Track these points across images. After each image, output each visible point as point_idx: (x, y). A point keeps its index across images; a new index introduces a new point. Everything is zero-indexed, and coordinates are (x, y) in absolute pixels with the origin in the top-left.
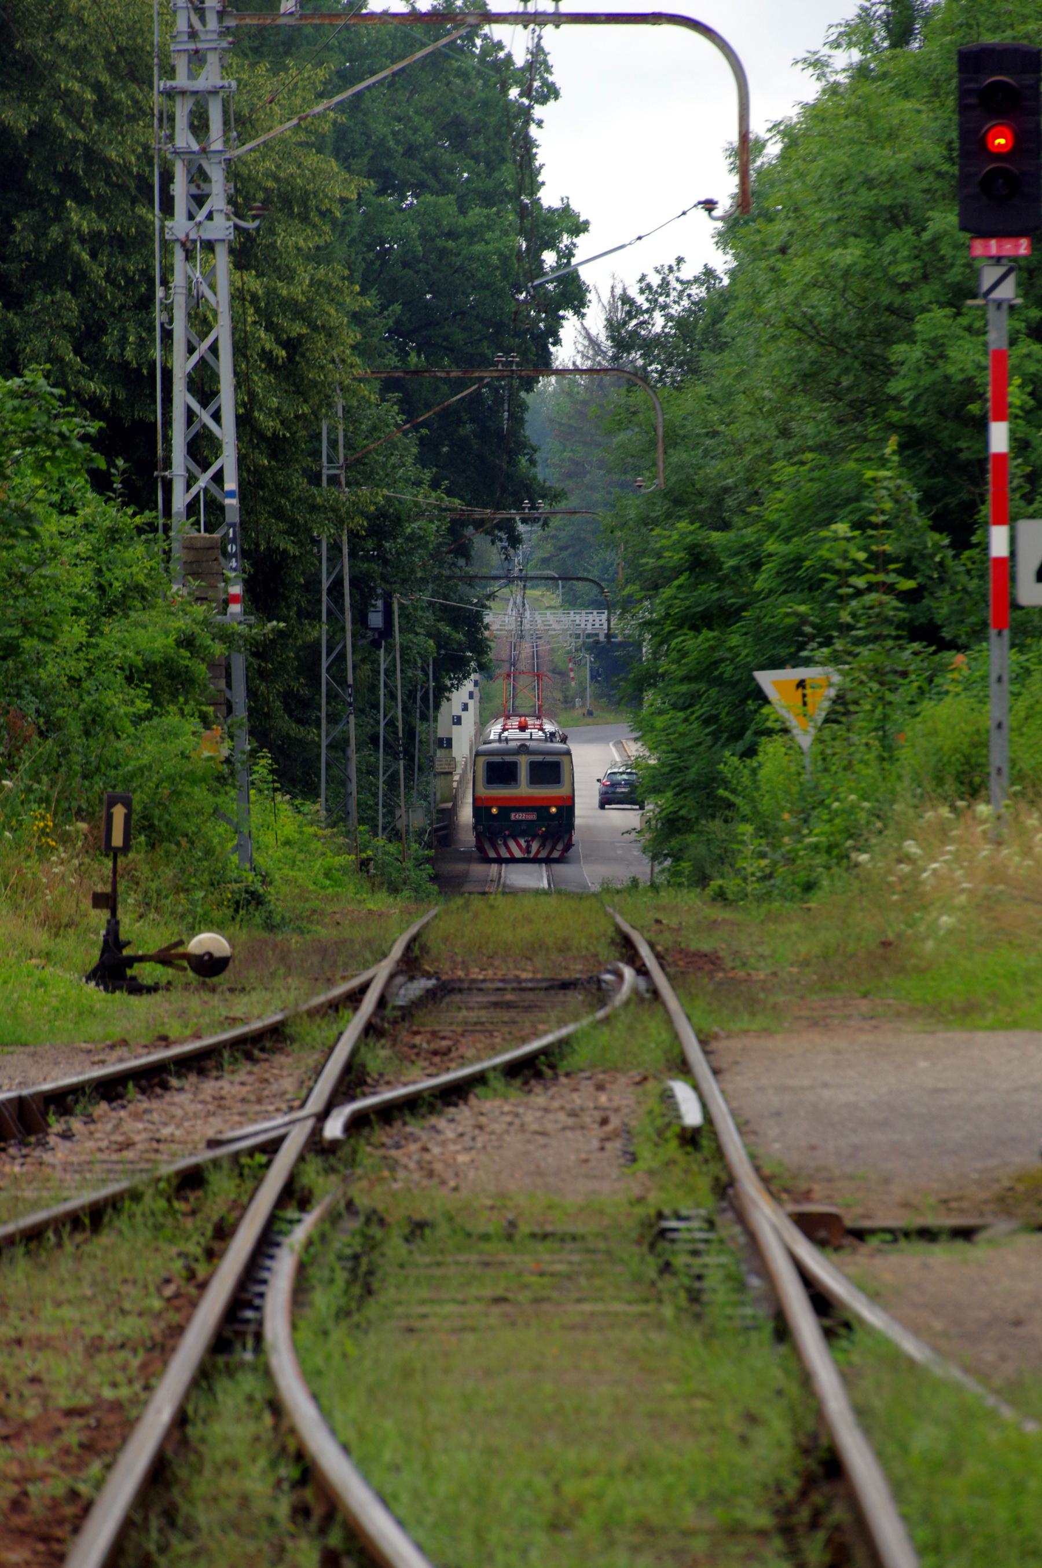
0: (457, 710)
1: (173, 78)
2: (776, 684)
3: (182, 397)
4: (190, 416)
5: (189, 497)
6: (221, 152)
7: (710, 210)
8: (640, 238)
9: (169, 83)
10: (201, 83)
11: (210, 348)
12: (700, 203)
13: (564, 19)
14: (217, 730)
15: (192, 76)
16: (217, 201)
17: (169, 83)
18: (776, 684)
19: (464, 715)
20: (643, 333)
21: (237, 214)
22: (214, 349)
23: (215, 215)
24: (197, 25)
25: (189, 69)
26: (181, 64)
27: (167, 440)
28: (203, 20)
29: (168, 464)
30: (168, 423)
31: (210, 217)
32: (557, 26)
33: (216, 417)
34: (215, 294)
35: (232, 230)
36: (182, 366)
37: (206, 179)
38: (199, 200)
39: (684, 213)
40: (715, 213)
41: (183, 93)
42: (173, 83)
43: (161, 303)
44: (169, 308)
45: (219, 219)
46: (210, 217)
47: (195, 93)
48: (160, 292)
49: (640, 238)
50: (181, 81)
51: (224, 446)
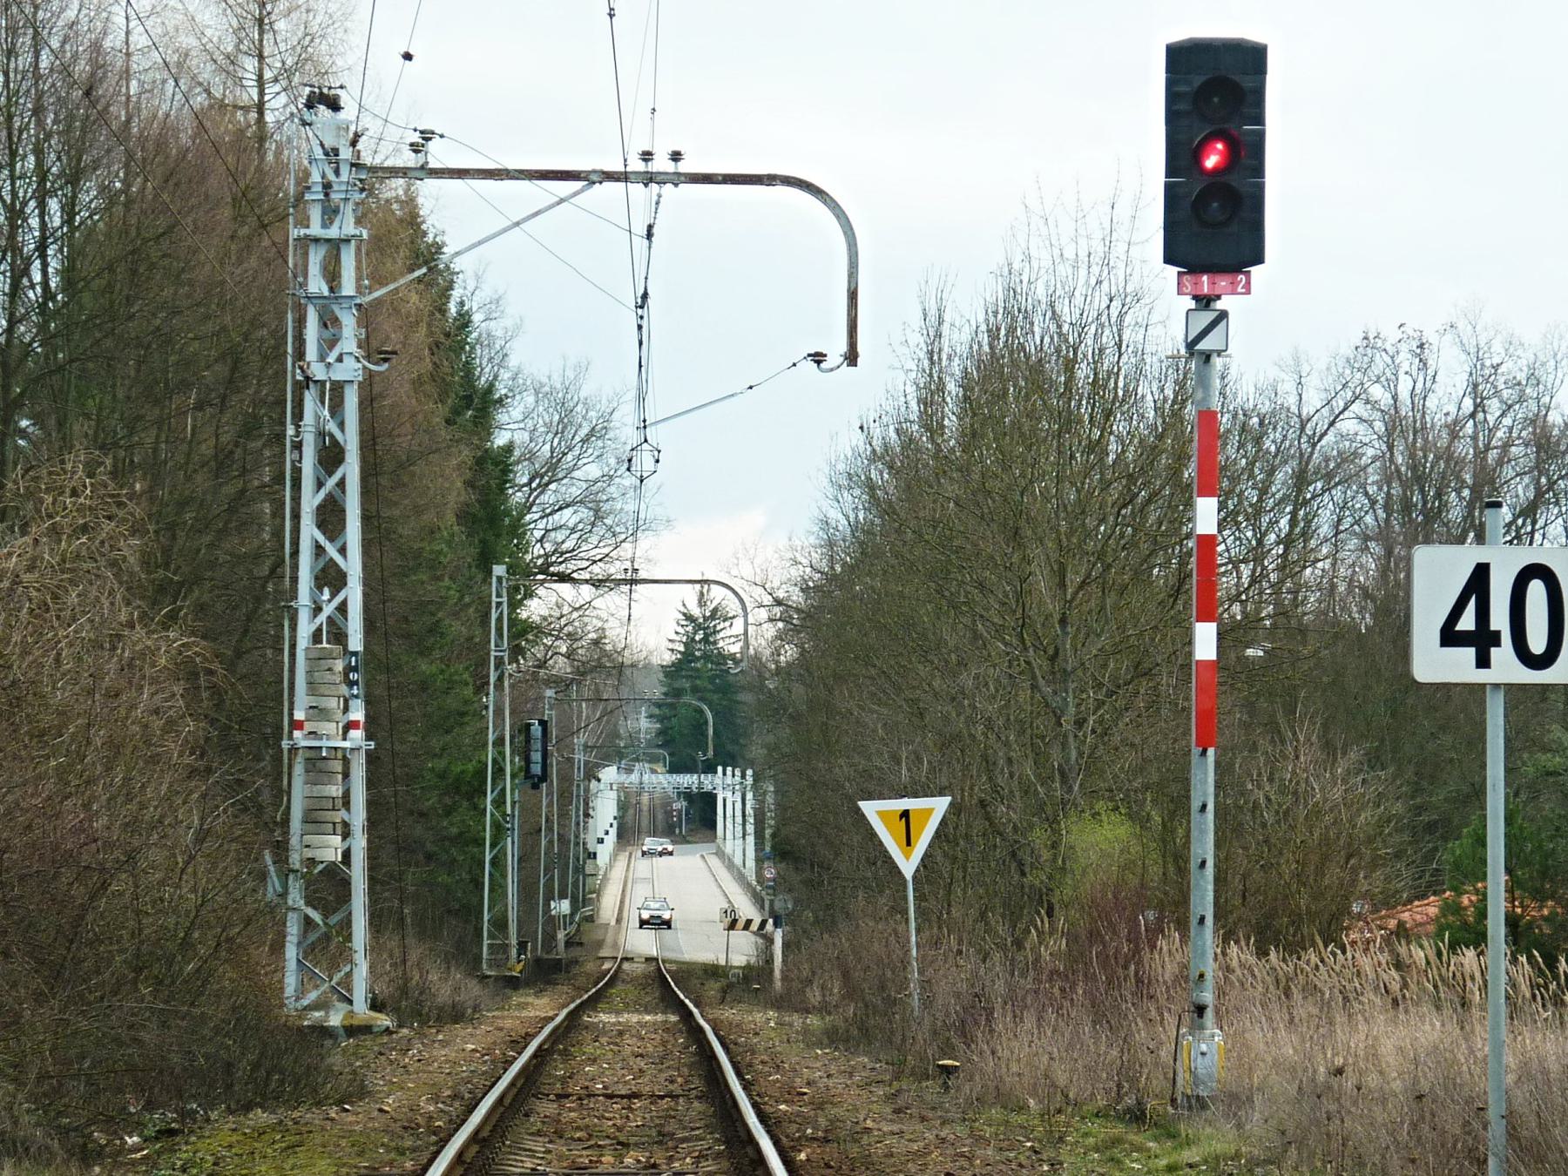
0: (601, 835)
1: (308, 227)
2: (882, 815)
3: (310, 532)
4: (319, 550)
5: (313, 627)
6: (351, 297)
7: (818, 362)
8: (751, 388)
9: (303, 232)
10: (333, 232)
11: (337, 485)
12: (809, 355)
13: (683, 179)
14: (348, 24)
15: (324, 226)
16: (349, 341)
17: (303, 232)
18: (882, 815)
19: (606, 837)
20: (306, 1023)
21: (368, 357)
22: (341, 484)
23: (345, 357)
24: (331, 177)
25: (323, 219)
26: (315, 214)
27: (295, 567)
28: (337, 172)
29: (295, 597)
30: (295, 553)
31: (340, 359)
32: (676, 185)
33: (343, 551)
34: (343, 431)
35: (360, 372)
36: (310, 501)
37: (336, 321)
38: (332, 342)
39: (794, 365)
40: (823, 365)
41: (316, 240)
42: (308, 232)
43: (292, 441)
44: (298, 446)
45: (349, 362)
46: (340, 359)
47: (328, 241)
48: (290, 431)
49: (751, 388)
50: (315, 229)
51: (349, 578)
